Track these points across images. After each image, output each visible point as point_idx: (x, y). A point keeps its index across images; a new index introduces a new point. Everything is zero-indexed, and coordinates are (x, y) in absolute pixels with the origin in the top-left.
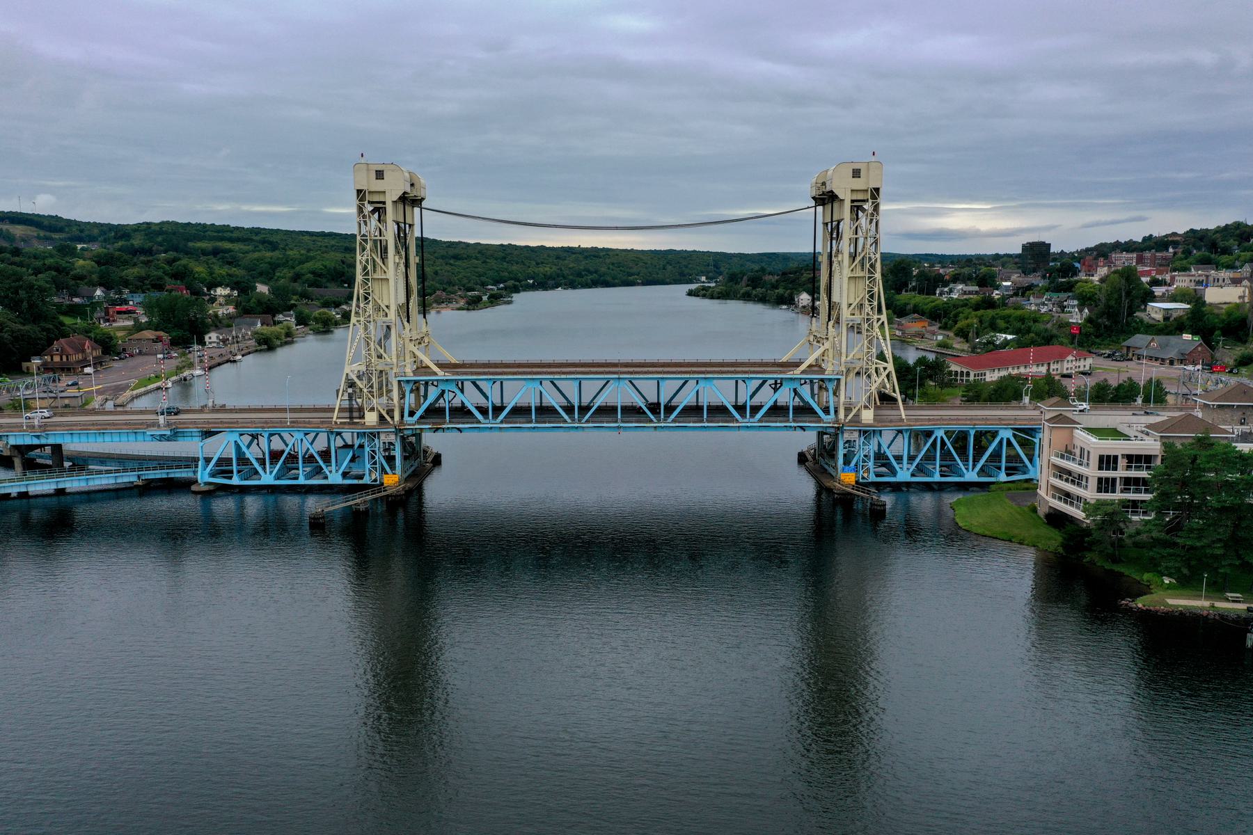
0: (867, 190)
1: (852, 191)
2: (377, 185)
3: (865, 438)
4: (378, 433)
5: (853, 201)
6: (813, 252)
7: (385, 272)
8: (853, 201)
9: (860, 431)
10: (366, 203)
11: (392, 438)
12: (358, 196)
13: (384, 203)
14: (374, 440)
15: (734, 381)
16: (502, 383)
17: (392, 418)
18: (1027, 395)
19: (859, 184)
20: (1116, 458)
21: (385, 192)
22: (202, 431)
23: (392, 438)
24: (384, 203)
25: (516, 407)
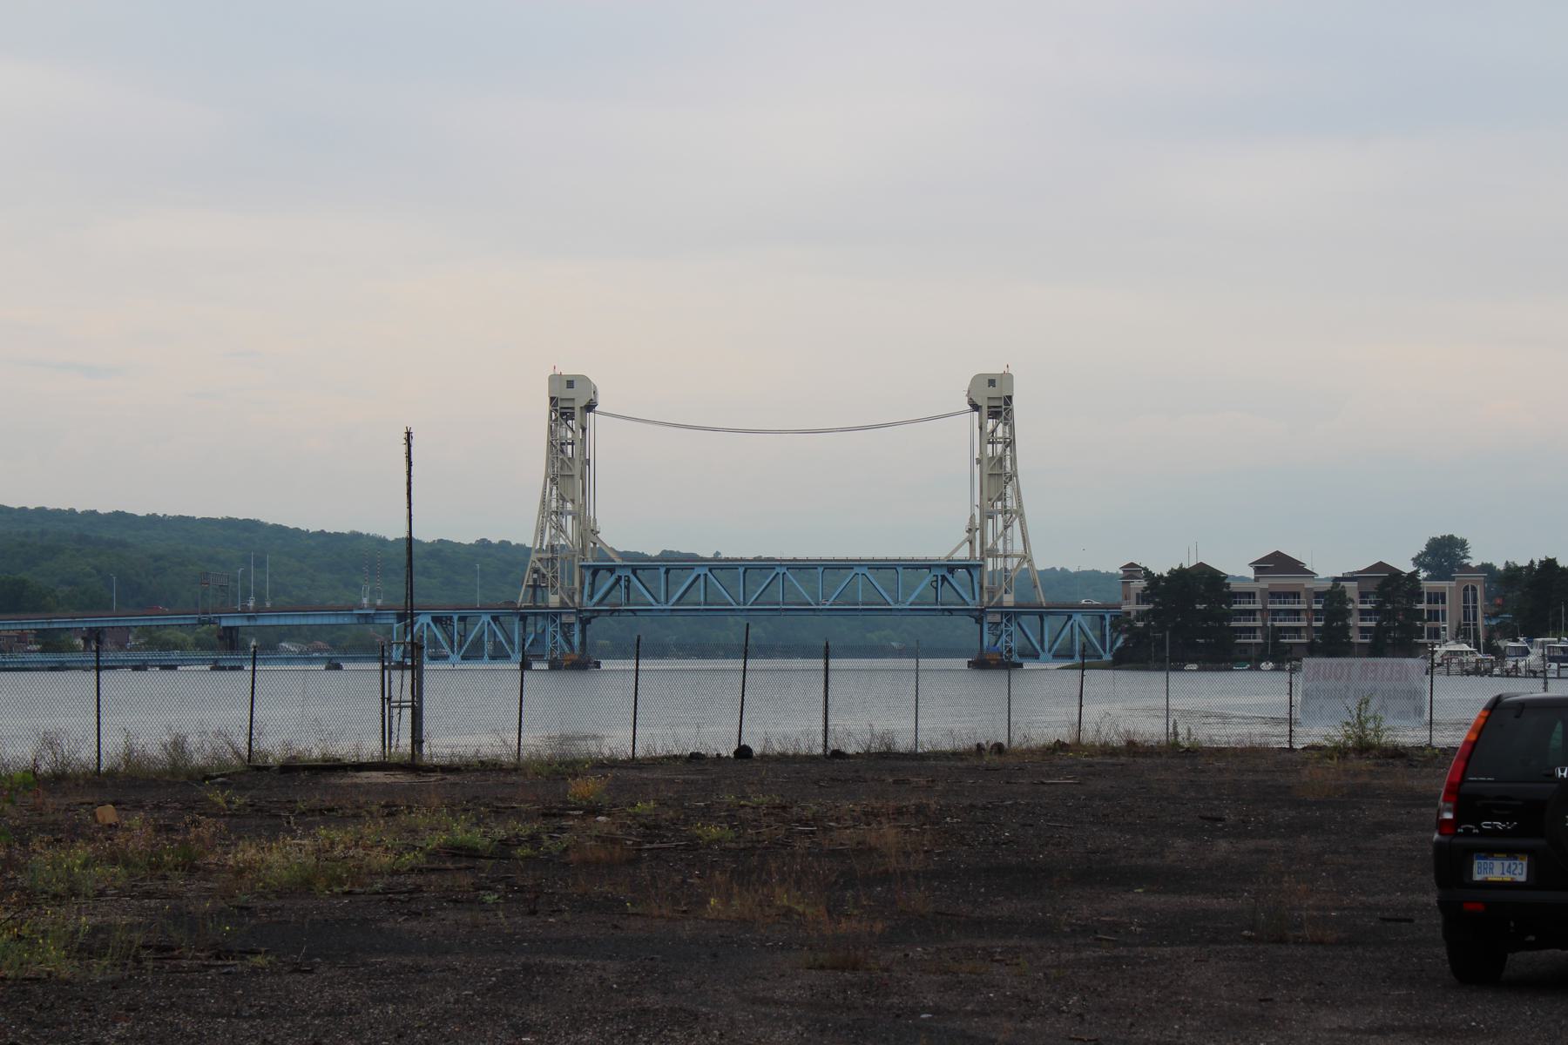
0: (1001, 398)
1: (989, 398)
2: (569, 393)
3: (1007, 621)
4: (561, 613)
5: (989, 407)
6: (640, 661)
7: (571, 469)
8: (989, 407)
9: (1002, 612)
10: (558, 408)
11: (573, 619)
12: (551, 404)
13: (573, 408)
14: (555, 621)
15: (631, 602)
16: (667, 572)
17: (573, 601)
18: (365, 597)
19: (993, 392)
21: (573, 399)
22: (398, 614)
23: (573, 619)
24: (573, 408)
25: (1079, 572)
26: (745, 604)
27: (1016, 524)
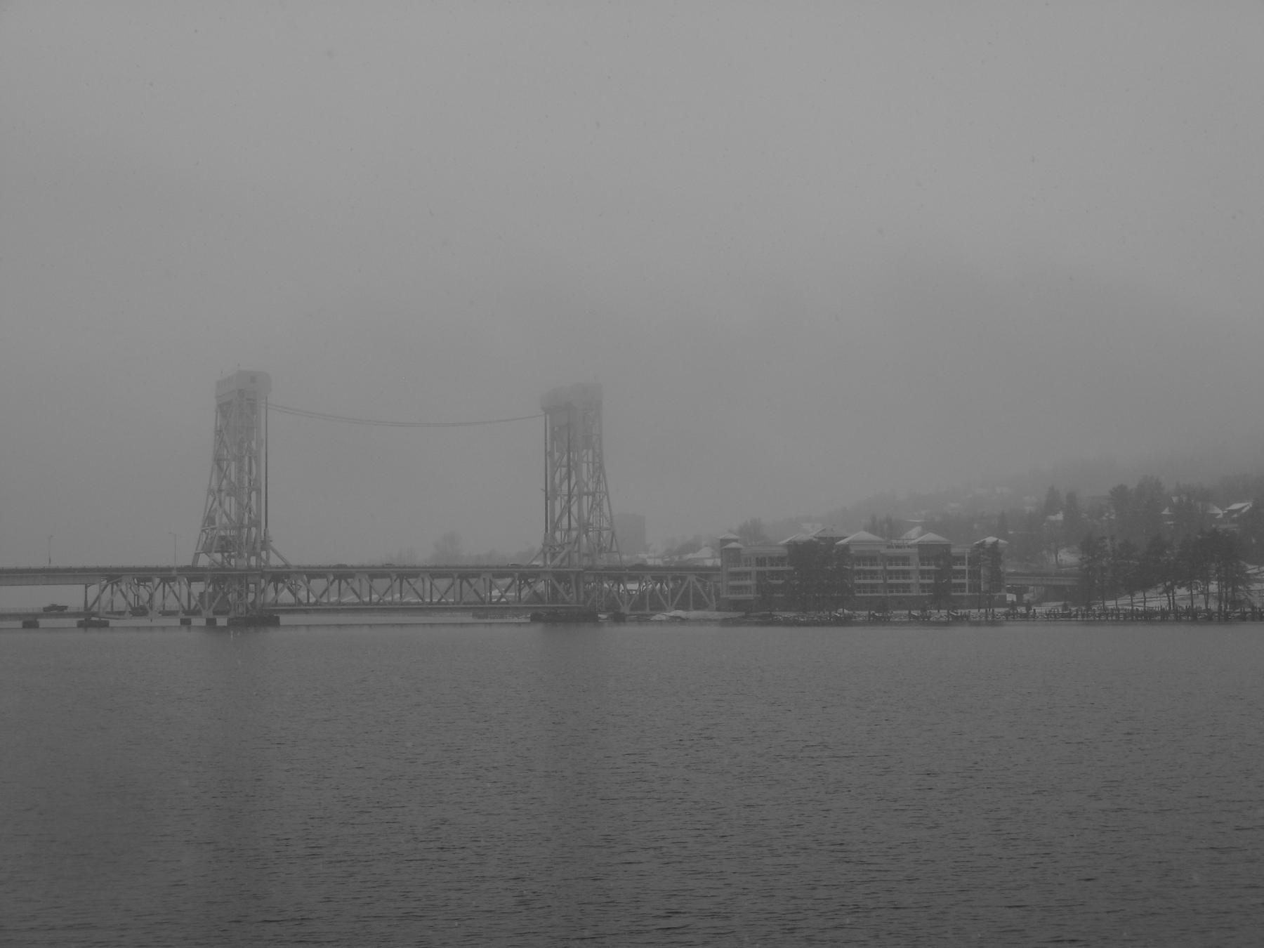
27: (605, 500)
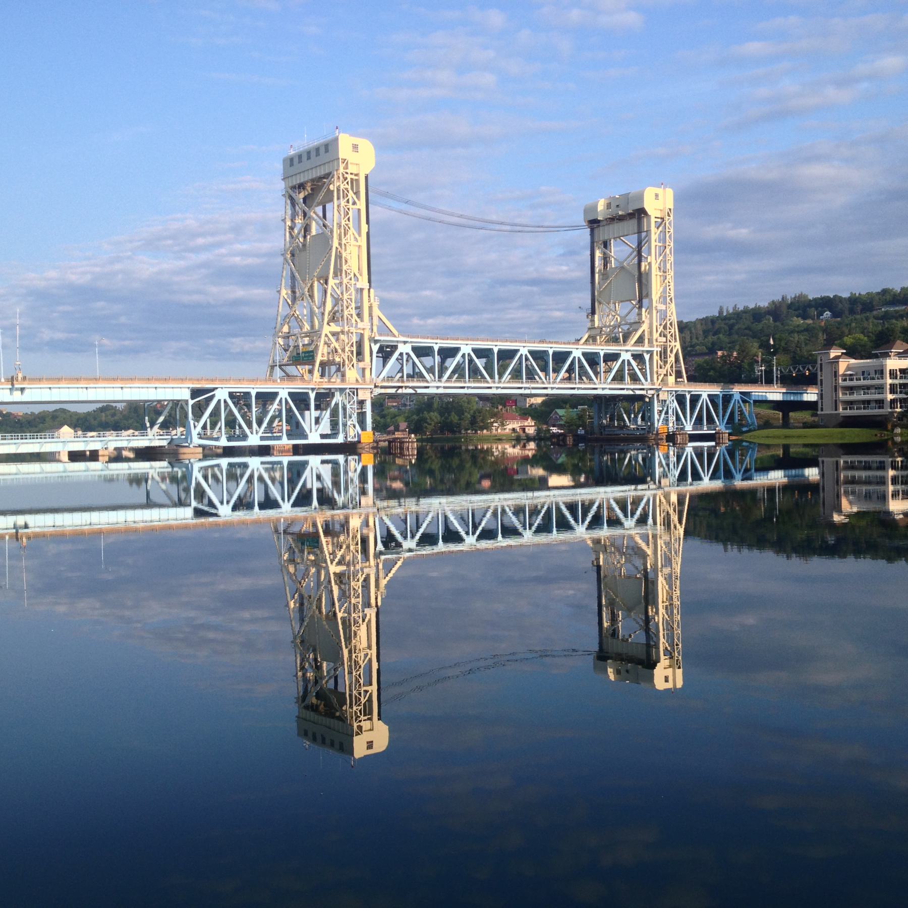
20: (896, 370)
26: (554, 383)
